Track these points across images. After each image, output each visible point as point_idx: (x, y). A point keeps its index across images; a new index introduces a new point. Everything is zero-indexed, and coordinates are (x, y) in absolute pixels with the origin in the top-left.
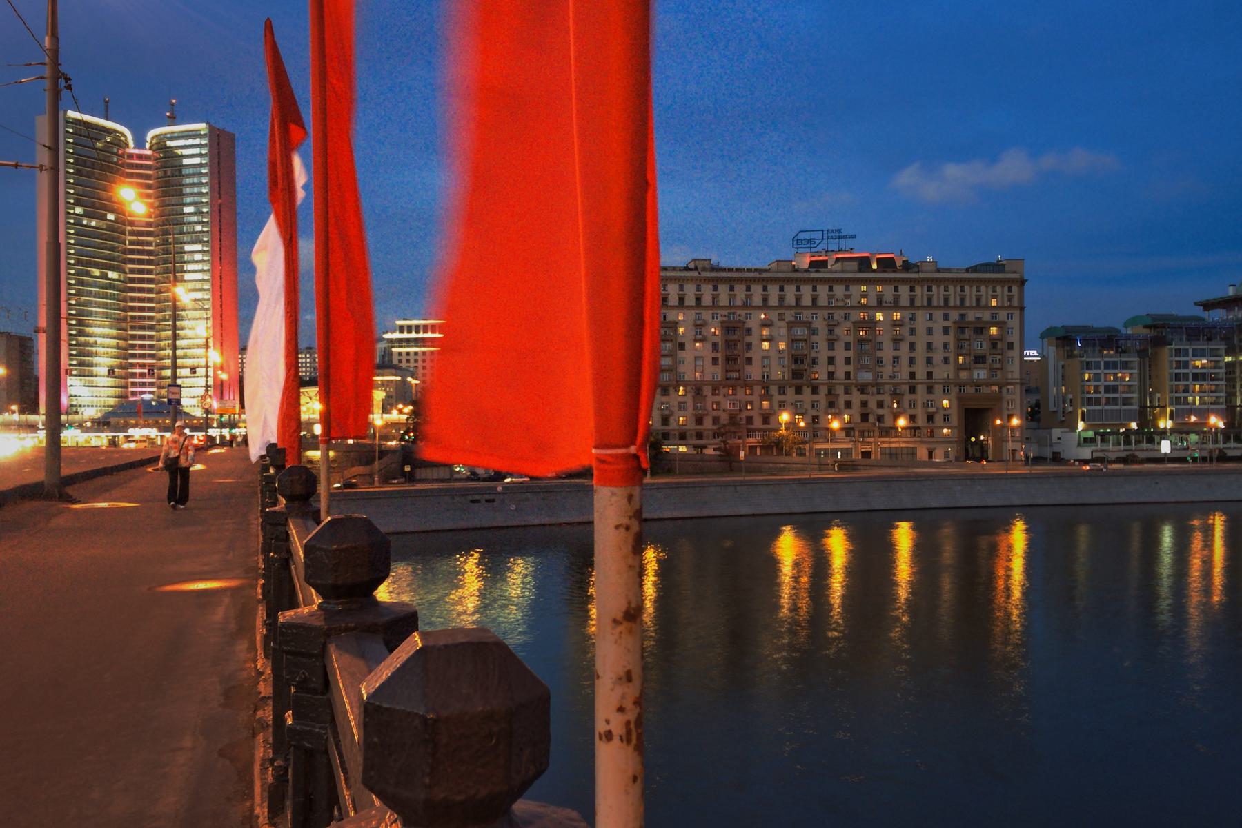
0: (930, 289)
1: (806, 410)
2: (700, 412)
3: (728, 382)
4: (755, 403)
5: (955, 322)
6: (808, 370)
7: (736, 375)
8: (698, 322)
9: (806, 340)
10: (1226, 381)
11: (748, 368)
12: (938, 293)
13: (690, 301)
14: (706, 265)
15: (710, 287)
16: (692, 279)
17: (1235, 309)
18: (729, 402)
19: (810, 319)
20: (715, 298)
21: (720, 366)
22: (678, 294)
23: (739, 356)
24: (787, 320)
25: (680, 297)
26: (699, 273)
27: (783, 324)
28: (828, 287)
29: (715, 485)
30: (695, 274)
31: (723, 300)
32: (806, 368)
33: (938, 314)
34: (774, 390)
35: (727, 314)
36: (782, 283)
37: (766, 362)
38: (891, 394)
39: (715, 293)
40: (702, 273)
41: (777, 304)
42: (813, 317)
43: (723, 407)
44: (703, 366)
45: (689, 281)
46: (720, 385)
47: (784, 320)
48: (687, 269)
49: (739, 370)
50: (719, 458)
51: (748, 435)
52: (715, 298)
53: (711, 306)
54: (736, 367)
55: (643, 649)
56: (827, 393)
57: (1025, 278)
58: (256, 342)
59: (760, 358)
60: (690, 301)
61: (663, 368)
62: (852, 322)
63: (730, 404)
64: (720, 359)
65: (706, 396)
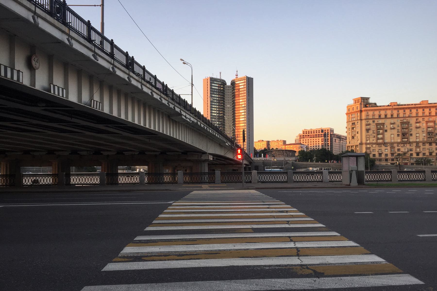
1: (433, 151)
2: (393, 152)
3: (404, 143)
4: (388, 149)
6: (434, 137)
7: (406, 140)
9: (433, 127)
11: (411, 137)
14: (396, 104)
15: (409, 110)
18: (403, 149)
19: (435, 120)
21: (400, 137)
22: (429, 112)
23: (407, 133)
24: (425, 121)
25: (380, 115)
26: (392, 107)
27: (424, 122)
28: (422, 109)
29: (277, 164)
30: (391, 107)
32: (433, 136)
34: (421, 144)
36: (423, 108)
37: (418, 135)
39: (398, 113)
40: (393, 107)
41: (384, 117)
43: (401, 150)
44: (394, 137)
45: (415, 108)
46: (426, 142)
47: (424, 121)
48: (388, 106)
49: (407, 138)
50: (396, 166)
51: (411, 159)
53: (397, 117)
54: (406, 137)
56: (416, 146)
59: (416, 134)
60: (389, 116)
61: (379, 138)
62: (376, 124)
63: (404, 149)
64: (400, 135)
65: (420, 146)
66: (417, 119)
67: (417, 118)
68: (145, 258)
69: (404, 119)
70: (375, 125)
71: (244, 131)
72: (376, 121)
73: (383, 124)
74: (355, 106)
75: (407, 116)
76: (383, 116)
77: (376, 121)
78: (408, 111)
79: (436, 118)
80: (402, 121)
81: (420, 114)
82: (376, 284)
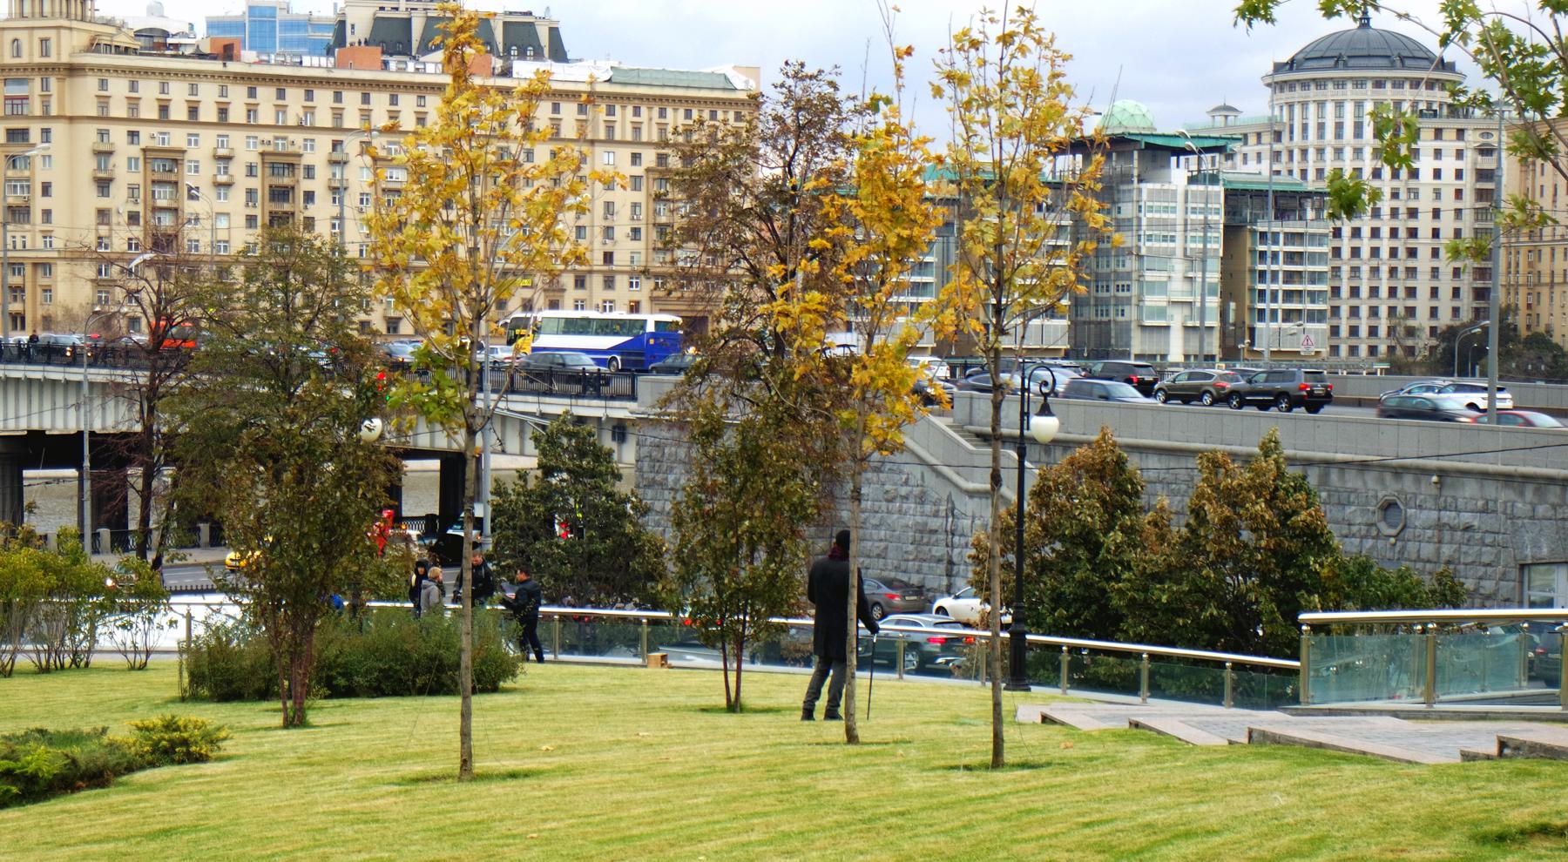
0: (637, 112)
5: (648, 170)
8: (222, 152)
10: (1450, 328)
12: (624, 118)
13: (208, 113)
16: (213, 76)
17: (1169, 162)
20: (252, 110)
31: (266, 115)
33: (118, 134)
35: (271, 139)
38: (545, 290)
42: (306, 146)
52: (252, 110)
55: (44, 670)
57: (1269, 90)
58: (372, 707)
60: (208, 113)
66: (336, 145)
67: (103, 126)
68: (733, 695)
69: (278, 134)
70: (140, 155)
71: (1542, 174)
72: (145, 132)
73: (174, 159)
74: (26, 32)
75: (292, 121)
76: (179, 112)
77: (145, 132)
78: (295, 95)
79: (277, 138)
80: (270, 149)
81: (352, 120)
82: (1554, 507)
